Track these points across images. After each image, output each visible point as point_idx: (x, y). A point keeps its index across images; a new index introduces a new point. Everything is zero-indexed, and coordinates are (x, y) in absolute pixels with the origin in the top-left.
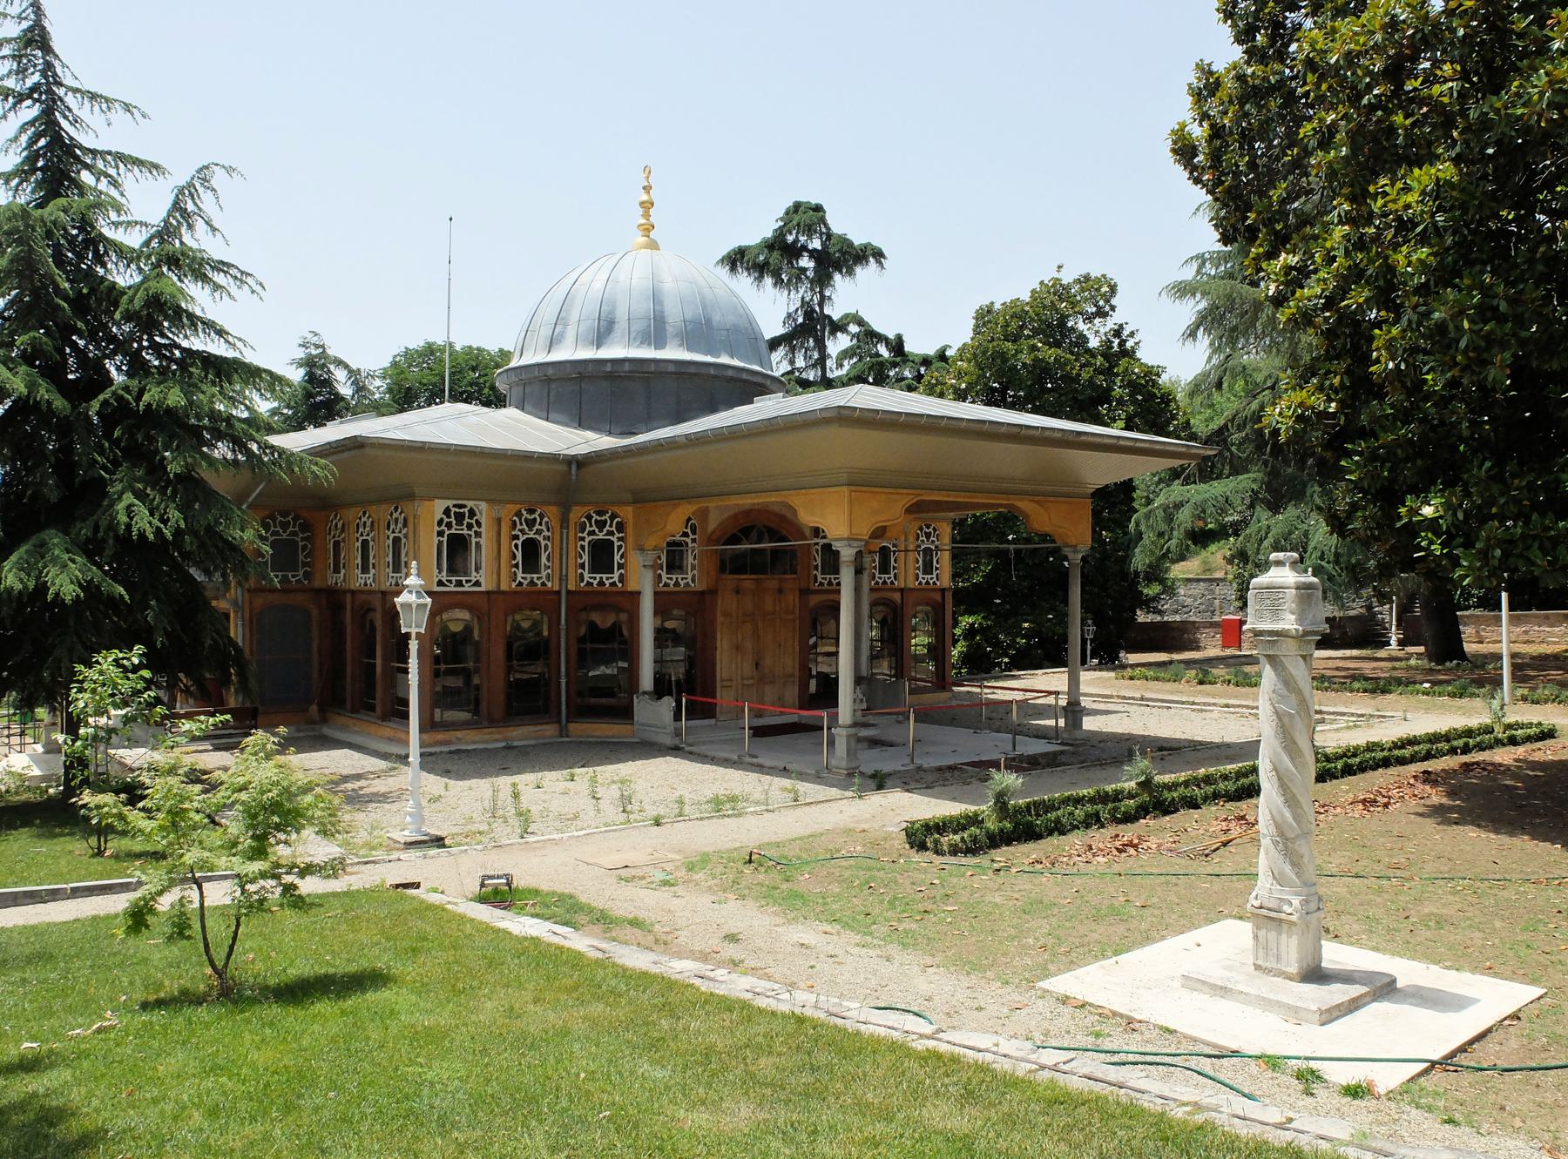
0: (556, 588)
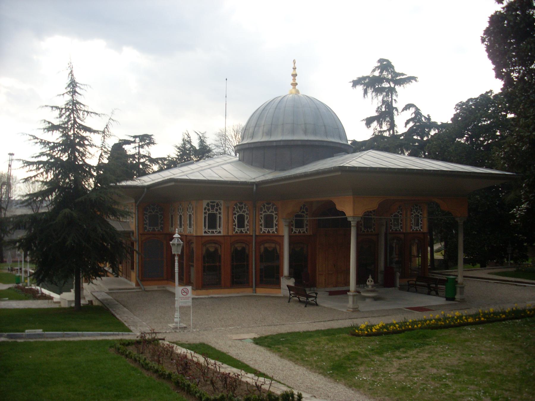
0: (251, 234)
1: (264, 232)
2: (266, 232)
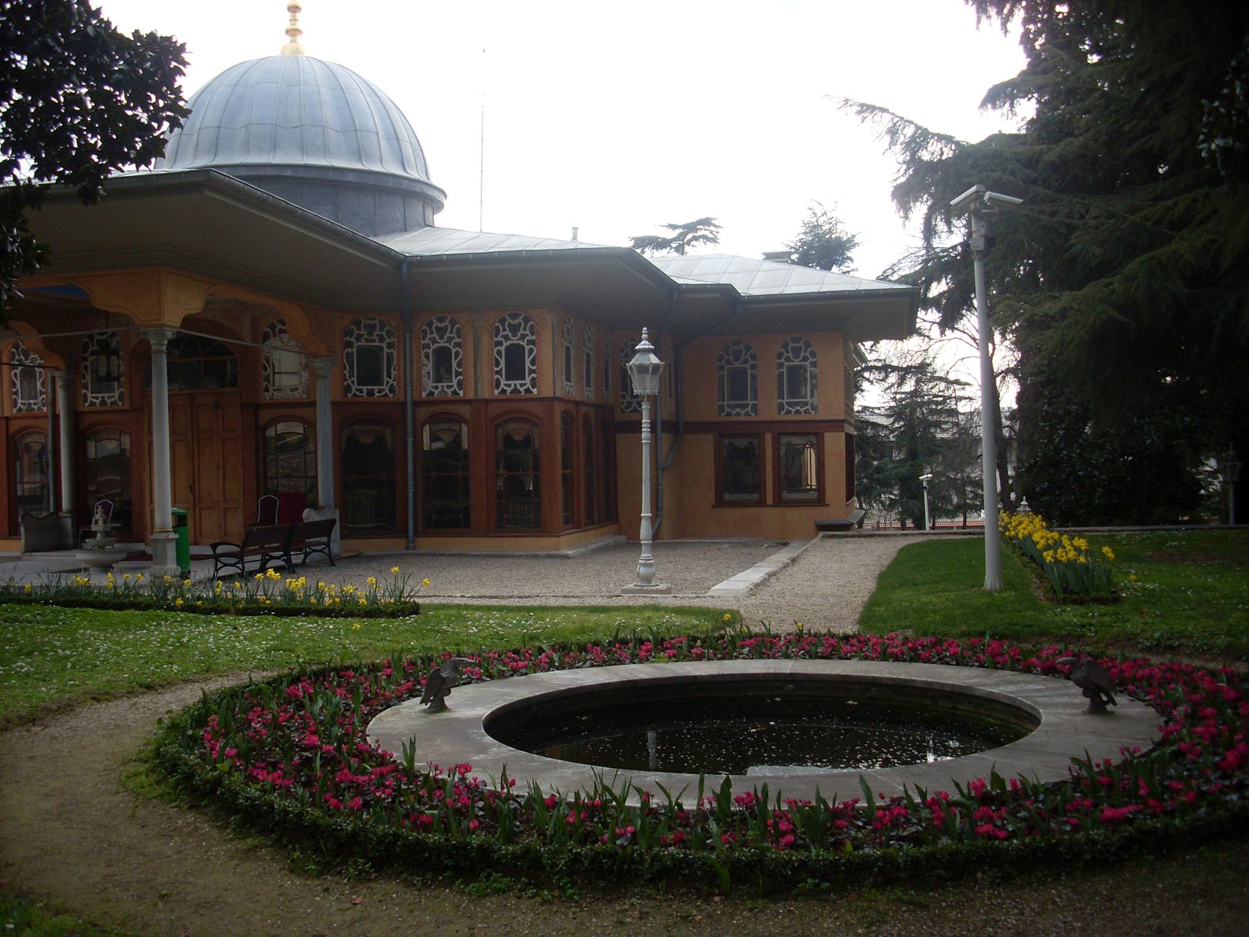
1: (92, 404)
2: (98, 402)
